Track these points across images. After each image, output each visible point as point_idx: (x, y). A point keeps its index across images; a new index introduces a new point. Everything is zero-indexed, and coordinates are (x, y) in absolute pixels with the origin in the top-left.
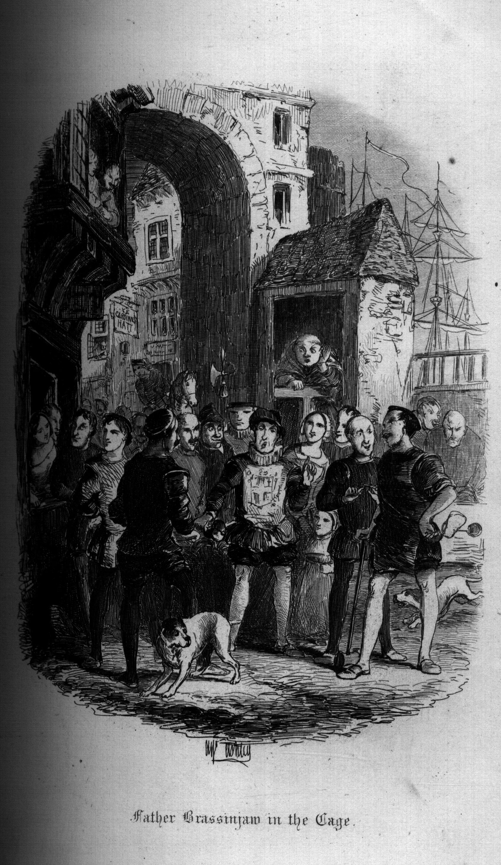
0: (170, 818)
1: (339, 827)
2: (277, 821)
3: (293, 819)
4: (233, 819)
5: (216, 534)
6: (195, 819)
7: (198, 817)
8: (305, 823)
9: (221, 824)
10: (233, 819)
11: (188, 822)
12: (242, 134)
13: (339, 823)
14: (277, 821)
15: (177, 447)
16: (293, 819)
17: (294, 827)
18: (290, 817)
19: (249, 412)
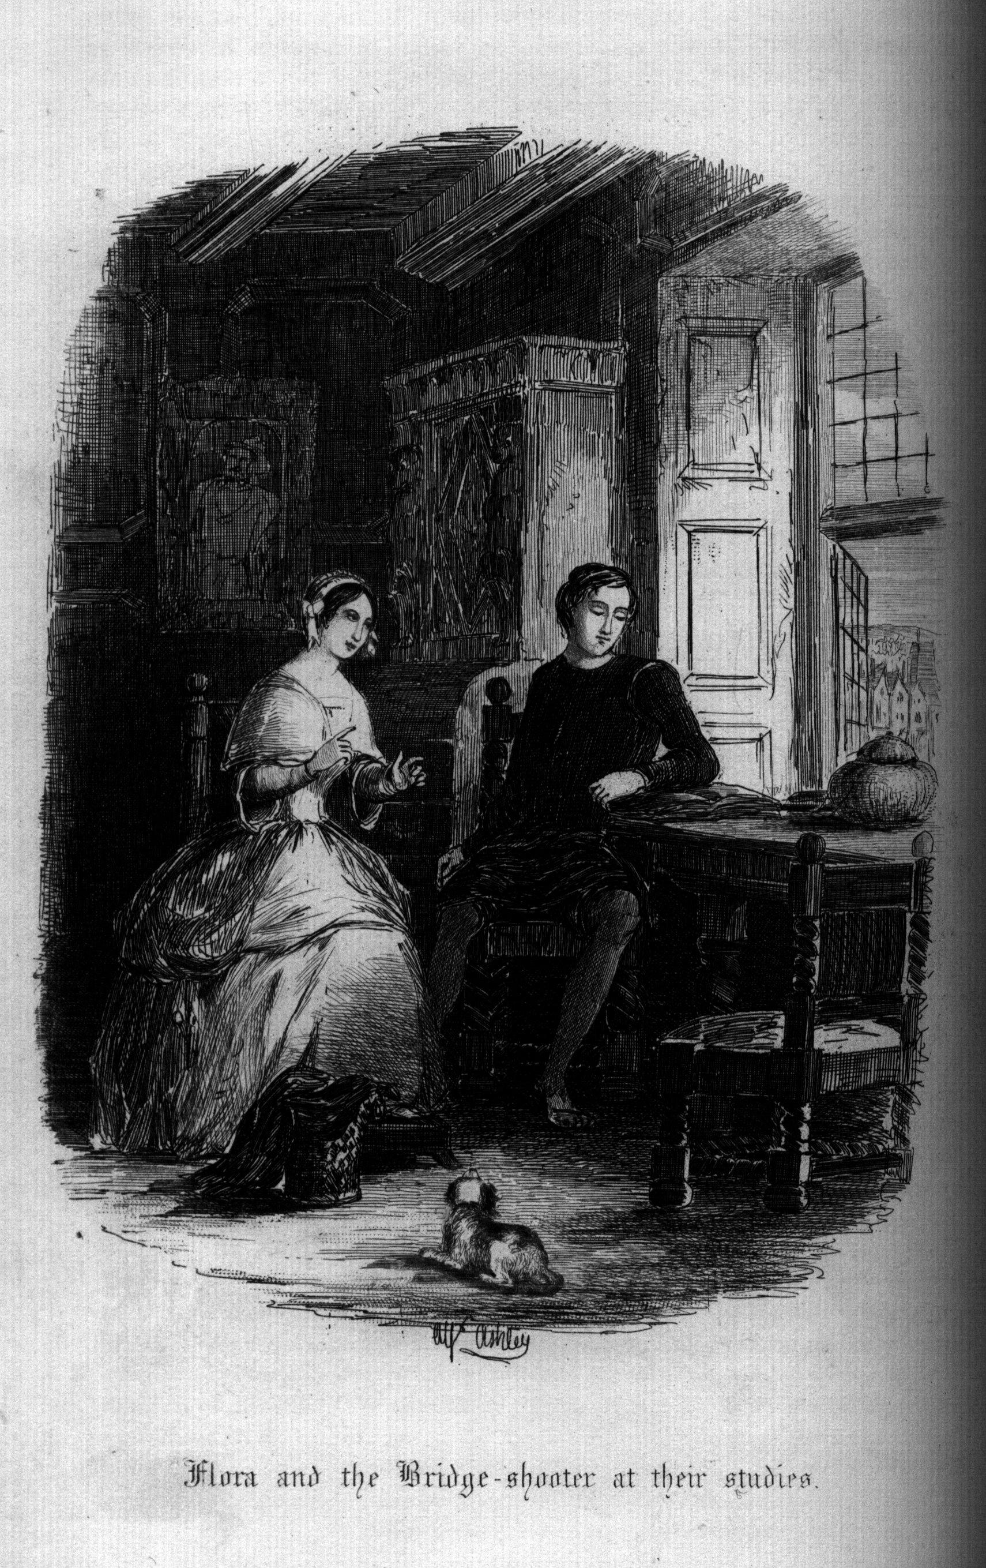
0: (584, 1478)
1: (469, 1489)
2: (355, 1478)
3: (350, 1477)
4: (298, 1478)
5: (741, 939)
6: (423, 1479)
7: (237, 1474)
8: (484, 1482)
9: (228, 1487)
10: (298, 1478)
11: (411, 1485)
12: (333, 711)
13: (468, 1482)
14: (623, 1480)
15: (207, 915)
16: (350, 1477)
17: (352, 1490)
18: (345, 1473)
19: (264, 928)
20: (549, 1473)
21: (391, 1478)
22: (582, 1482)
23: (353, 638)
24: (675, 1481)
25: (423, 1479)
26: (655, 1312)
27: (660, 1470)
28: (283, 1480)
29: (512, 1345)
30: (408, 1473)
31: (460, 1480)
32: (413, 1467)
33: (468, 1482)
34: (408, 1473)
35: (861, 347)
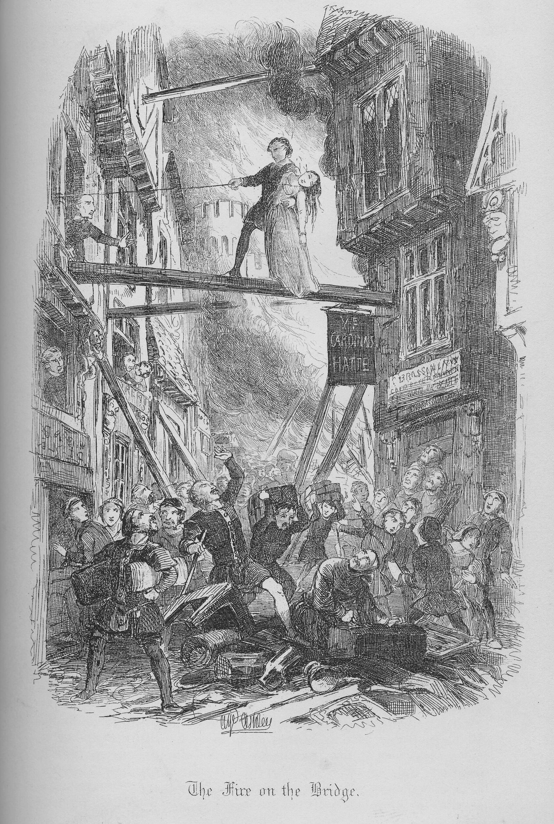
3: (286, 790)
4: (271, 791)
6: (323, 792)
16: (286, 790)
20: (266, 788)
21: (306, 791)
22: (244, 792)
23: (400, 388)
24: (294, 793)
25: (323, 792)
26: (491, 662)
27: (286, 787)
28: (248, 790)
29: (265, 724)
30: (316, 789)
31: (341, 792)
32: (318, 785)
33: (345, 794)
34: (316, 789)
35: (195, 185)
